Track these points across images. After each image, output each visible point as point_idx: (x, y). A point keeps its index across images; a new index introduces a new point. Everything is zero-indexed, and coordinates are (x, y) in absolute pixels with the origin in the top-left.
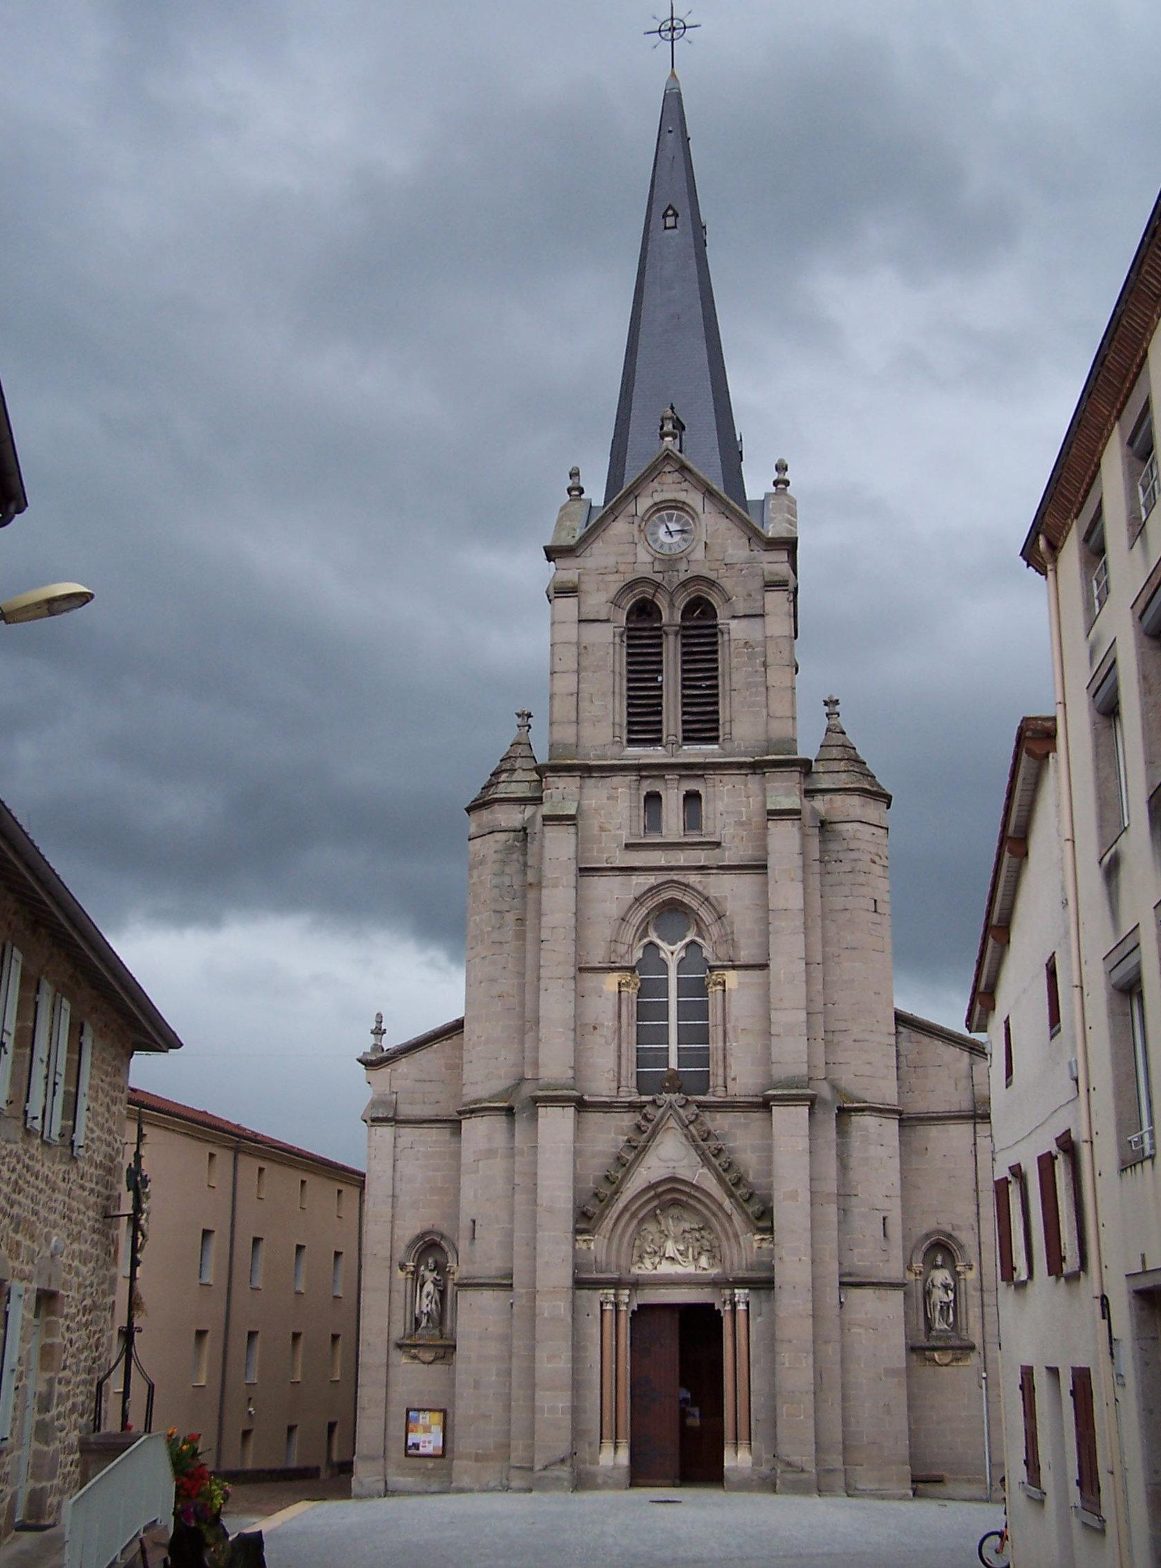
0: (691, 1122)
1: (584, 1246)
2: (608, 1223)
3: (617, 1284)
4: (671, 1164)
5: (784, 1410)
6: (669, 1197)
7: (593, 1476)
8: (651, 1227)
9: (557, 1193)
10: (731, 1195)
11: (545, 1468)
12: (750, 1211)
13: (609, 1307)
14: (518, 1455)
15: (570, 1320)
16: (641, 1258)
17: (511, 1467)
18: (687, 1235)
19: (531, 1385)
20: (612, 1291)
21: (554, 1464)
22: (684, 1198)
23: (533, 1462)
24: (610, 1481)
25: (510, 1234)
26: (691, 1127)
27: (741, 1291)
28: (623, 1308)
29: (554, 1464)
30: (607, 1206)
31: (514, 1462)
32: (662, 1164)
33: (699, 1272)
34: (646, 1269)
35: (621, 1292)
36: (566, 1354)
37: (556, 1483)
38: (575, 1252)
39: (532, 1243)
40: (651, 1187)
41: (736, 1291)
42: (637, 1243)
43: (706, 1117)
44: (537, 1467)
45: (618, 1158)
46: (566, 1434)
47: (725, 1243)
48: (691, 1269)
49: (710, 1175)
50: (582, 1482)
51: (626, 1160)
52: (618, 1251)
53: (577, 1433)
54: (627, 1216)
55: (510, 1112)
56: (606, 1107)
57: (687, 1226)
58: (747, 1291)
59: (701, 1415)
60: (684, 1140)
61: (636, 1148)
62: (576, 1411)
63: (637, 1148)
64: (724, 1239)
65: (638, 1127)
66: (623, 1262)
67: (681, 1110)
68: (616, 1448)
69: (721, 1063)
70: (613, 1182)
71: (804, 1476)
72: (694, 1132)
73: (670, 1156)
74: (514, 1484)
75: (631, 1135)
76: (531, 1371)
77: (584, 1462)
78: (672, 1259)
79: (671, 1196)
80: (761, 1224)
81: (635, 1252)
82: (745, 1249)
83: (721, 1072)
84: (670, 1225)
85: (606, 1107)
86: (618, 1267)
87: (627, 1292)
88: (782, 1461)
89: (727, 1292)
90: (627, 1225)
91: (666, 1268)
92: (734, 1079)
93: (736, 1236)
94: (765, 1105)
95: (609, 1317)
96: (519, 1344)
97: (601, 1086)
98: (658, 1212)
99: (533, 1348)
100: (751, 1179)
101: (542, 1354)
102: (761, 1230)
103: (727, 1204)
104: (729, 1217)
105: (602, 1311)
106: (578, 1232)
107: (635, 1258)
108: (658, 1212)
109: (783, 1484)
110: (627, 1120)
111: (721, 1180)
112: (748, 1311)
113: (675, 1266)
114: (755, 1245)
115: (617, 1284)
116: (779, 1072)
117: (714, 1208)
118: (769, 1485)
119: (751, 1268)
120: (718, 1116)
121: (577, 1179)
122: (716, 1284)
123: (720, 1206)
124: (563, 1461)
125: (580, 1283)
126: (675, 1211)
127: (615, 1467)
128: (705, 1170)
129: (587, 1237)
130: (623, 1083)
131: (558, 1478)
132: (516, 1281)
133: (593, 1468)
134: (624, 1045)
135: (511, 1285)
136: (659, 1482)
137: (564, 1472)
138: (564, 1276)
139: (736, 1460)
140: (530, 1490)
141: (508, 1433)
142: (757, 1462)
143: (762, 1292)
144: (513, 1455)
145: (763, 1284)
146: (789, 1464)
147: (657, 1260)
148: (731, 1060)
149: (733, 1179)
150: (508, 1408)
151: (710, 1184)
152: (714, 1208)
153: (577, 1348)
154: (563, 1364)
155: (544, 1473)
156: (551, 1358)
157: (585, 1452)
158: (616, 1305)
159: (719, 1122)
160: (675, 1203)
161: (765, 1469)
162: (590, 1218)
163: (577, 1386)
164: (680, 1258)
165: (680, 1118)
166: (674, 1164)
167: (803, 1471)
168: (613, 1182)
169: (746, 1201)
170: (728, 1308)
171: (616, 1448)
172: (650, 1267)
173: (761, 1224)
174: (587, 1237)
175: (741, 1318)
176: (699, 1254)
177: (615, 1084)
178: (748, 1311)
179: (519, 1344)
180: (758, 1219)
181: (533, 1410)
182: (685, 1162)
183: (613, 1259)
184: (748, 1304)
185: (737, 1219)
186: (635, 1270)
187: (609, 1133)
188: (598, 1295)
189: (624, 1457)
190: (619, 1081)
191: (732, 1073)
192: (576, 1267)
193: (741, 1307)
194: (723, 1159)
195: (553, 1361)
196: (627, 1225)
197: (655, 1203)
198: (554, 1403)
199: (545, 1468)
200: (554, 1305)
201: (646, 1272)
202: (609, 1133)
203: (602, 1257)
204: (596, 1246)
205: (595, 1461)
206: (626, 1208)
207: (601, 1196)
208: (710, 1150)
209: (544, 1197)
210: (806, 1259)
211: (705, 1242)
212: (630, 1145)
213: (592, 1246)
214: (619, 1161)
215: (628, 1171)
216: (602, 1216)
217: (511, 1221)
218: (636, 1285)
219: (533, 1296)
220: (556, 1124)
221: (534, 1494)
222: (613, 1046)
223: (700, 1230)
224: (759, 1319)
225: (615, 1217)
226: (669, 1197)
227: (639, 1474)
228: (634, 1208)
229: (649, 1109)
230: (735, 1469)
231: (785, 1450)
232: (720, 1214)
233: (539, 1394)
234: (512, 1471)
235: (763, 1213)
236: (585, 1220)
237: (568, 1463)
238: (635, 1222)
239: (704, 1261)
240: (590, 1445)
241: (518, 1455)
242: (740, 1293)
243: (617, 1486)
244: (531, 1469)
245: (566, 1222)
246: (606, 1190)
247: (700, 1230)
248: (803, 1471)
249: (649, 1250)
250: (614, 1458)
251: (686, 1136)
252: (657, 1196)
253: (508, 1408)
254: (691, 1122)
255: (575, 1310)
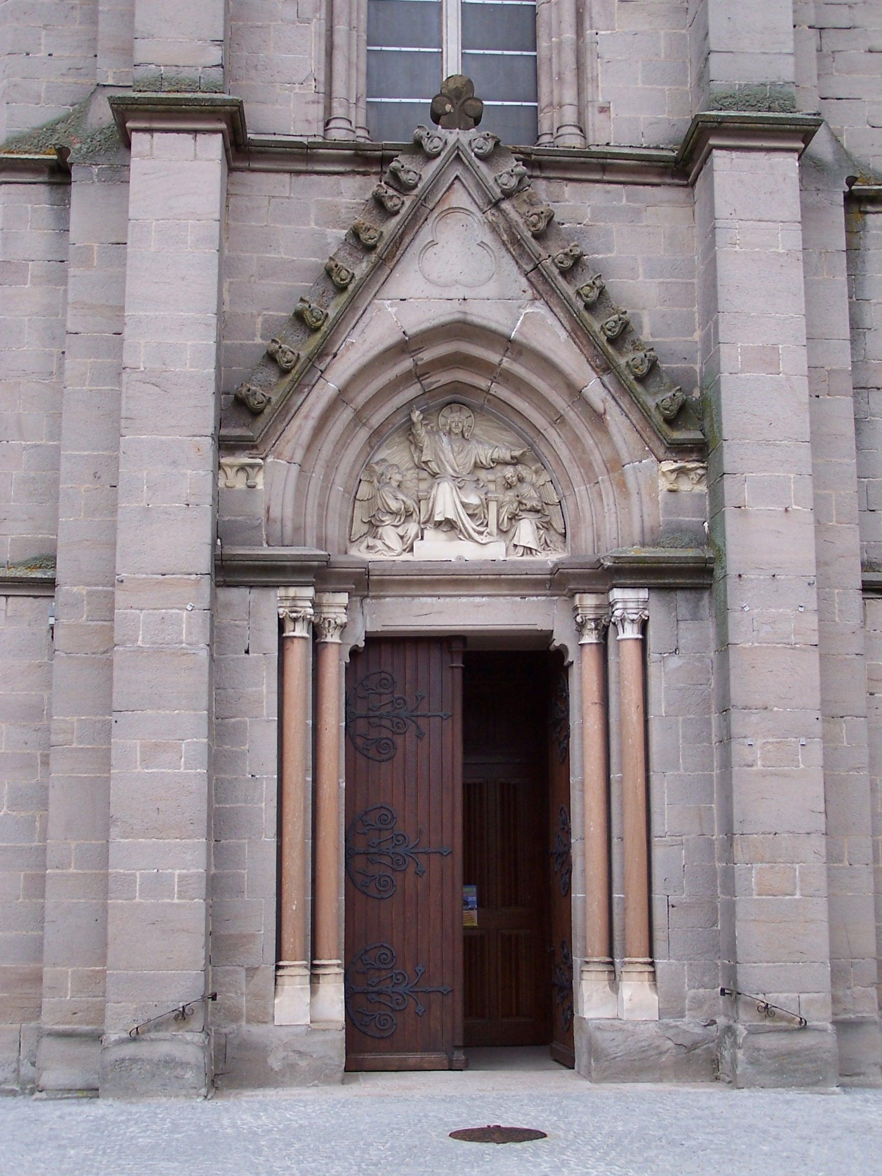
0: (508, 195)
1: (239, 482)
2: (300, 428)
3: (320, 574)
4: (458, 292)
5: (752, 876)
6: (443, 378)
7: (260, 1051)
8: (395, 454)
9: (176, 335)
10: (605, 367)
11: (135, 1037)
12: (651, 403)
13: (300, 631)
14: (60, 1004)
15: (204, 654)
16: (373, 526)
17: (42, 1034)
18: (483, 475)
19: (101, 820)
20: (309, 592)
21: (158, 1025)
22: (482, 383)
23: (100, 1014)
24: (303, 1063)
25: (53, 459)
26: (506, 205)
27: (629, 594)
28: (332, 637)
29: (158, 1025)
30: (299, 386)
31: (49, 1022)
32: (435, 292)
33: (516, 557)
34: (386, 549)
35: (328, 598)
36: (195, 743)
37: (163, 1076)
38: (218, 497)
39: (108, 481)
40: (405, 346)
41: (617, 594)
42: (364, 491)
43: (541, 188)
44: (113, 1036)
45: (329, 272)
46: (192, 948)
47: (581, 489)
48: (495, 551)
49: (551, 320)
50: (229, 1068)
51: (343, 288)
52: (323, 507)
53: (220, 945)
54: (345, 415)
55: (58, 173)
56: (298, 157)
57: (484, 453)
58: (643, 594)
59: (480, 903)
60: (488, 238)
61: (370, 249)
62: (218, 887)
63: (377, 248)
64: (575, 473)
65: (379, 202)
66: (334, 530)
67: (483, 168)
68: (314, 979)
69: (570, 76)
70: (315, 326)
71: (804, 1040)
72: (513, 215)
73: (452, 272)
74: (49, 1078)
75: (359, 219)
76: (99, 789)
77: (234, 1015)
78: (449, 525)
79: (452, 375)
80: (678, 435)
81: (360, 514)
82: (635, 497)
83: (569, 95)
84: (447, 453)
85: (298, 157)
86: (322, 542)
87: (343, 598)
88: (750, 1004)
89: (590, 600)
90: (342, 444)
91: (435, 548)
92: (604, 110)
93: (615, 465)
94: (682, 164)
95: (299, 655)
96: (68, 723)
97: (285, 112)
98: (416, 416)
99: (106, 731)
100: (646, 335)
101: (128, 743)
102: (678, 449)
103: (595, 390)
104: (598, 419)
105: (283, 642)
106: (225, 445)
107: (359, 528)
108: (416, 416)
109: (753, 1062)
110: (350, 193)
111: (579, 331)
112: (643, 643)
113: (458, 545)
114: (663, 484)
115: (320, 574)
116: (728, 74)
117: (560, 401)
118: (704, 1061)
119: (652, 538)
120: (568, 190)
121: (225, 324)
122: (559, 583)
123: (576, 393)
124: (182, 1016)
125: (229, 571)
126: (455, 418)
127: (315, 1026)
128: (540, 309)
129: (245, 460)
130: (338, 111)
131: (169, 1062)
132: (62, 573)
133: (256, 1031)
134: (341, 28)
135: (51, 584)
136: (413, 1058)
137: (187, 1046)
138: (195, 549)
139: (610, 1001)
140: (92, 1092)
141: (37, 949)
142: (671, 1008)
143: (680, 596)
144: (48, 1002)
145: (689, 575)
146: (767, 1010)
147: (412, 528)
148: (595, 67)
149: (610, 338)
150: (37, 885)
151: (550, 335)
152: (560, 401)
153: (221, 727)
154: (186, 766)
155: (130, 1050)
156: (152, 752)
157: (238, 995)
158: (316, 631)
159: (576, 204)
160: (457, 398)
161: (691, 1025)
162: (256, 413)
163: (220, 826)
164: (470, 524)
165: (481, 185)
166: (461, 292)
167: (803, 1027)
168: (315, 326)
169: (641, 380)
170: (590, 638)
171: (314, 979)
172: (397, 545)
173: (678, 435)
174: (245, 460)
175: (626, 659)
176: (514, 518)
177: (318, 111)
178: (643, 643)
179: (68, 723)
180: (671, 422)
181: (103, 885)
182: (490, 289)
183: (311, 519)
184: (644, 626)
185: (618, 423)
186: (360, 553)
187: (313, 216)
188: (270, 604)
189: (332, 999)
190: (328, 109)
191: (600, 94)
192: (221, 532)
193: (630, 632)
194: (584, 280)
195: (160, 757)
196: (342, 444)
197: (414, 391)
198: (163, 867)
199: (135, 1037)
200: (166, 614)
201: (387, 556)
202: (313, 216)
203: (284, 508)
204: (274, 485)
205: (264, 1016)
206: (341, 398)
207: (282, 359)
208: (556, 268)
209: (140, 350)
210: (803, 511)
211: (526, 490)
212: (358, 241)
213: (260, 480)
214: (333, 279)
215: (351, 305)
216: (285, 411)
217: (56, 433)
218: (364, 583)
219: (106, 608)
220: (178, 171)
221: (102, 1108)
222: (317, 26)
223: (515, 462)
224: (674, 662)
225: (316, 413)
226: (443, 378)
227: (371, 1043)
228: (361, 399)
229: (403, 162)
230: (616, 1024)
231: (756, 977)
232: (571, 415)
233: (119, 842)
234: (46, 1041)
235: (683, 408)
236: (242, 419)
237: (197, 1023)
238: (363, 435)
239: (526, 532)
240: (252, 971)
241: (60, 1004)
242: (627, 600)
243: (319, 1076)
244: (96, 1037)
245: (197, 415)
246: (300, 347)
247: (515, 462)
248: (803, 1027)
249: (394, 505)
250: (309, 1006)
251: (494, 228)
252: (416, 375)
253: (37, 885)
254: (508, 195)
255: (217, 639)
